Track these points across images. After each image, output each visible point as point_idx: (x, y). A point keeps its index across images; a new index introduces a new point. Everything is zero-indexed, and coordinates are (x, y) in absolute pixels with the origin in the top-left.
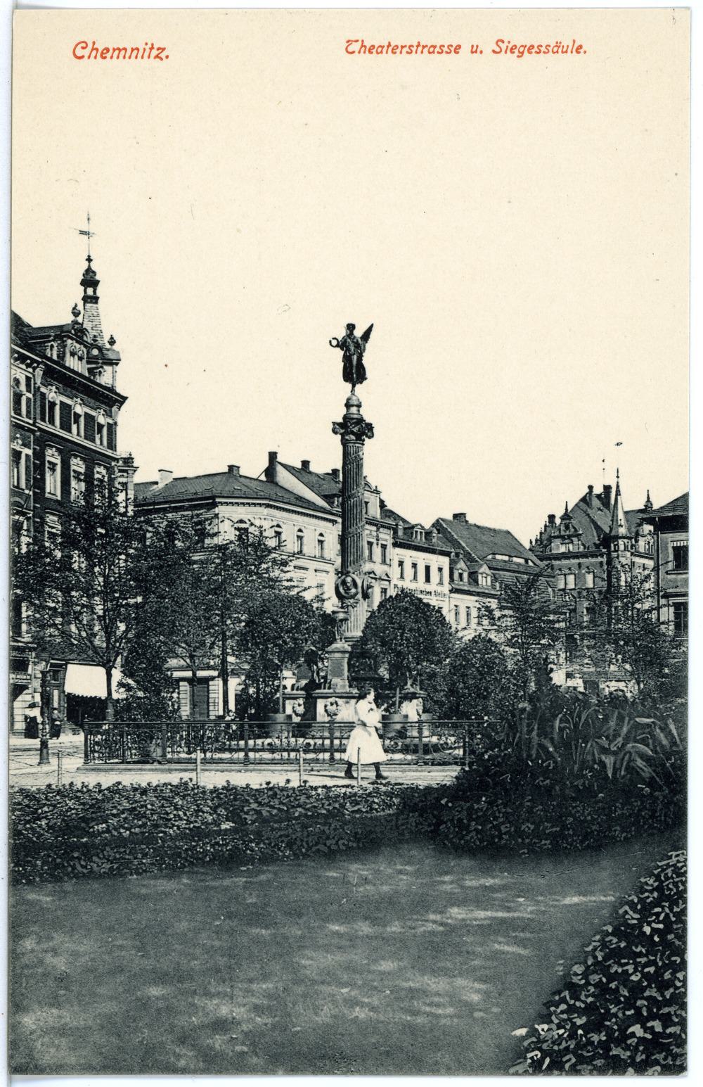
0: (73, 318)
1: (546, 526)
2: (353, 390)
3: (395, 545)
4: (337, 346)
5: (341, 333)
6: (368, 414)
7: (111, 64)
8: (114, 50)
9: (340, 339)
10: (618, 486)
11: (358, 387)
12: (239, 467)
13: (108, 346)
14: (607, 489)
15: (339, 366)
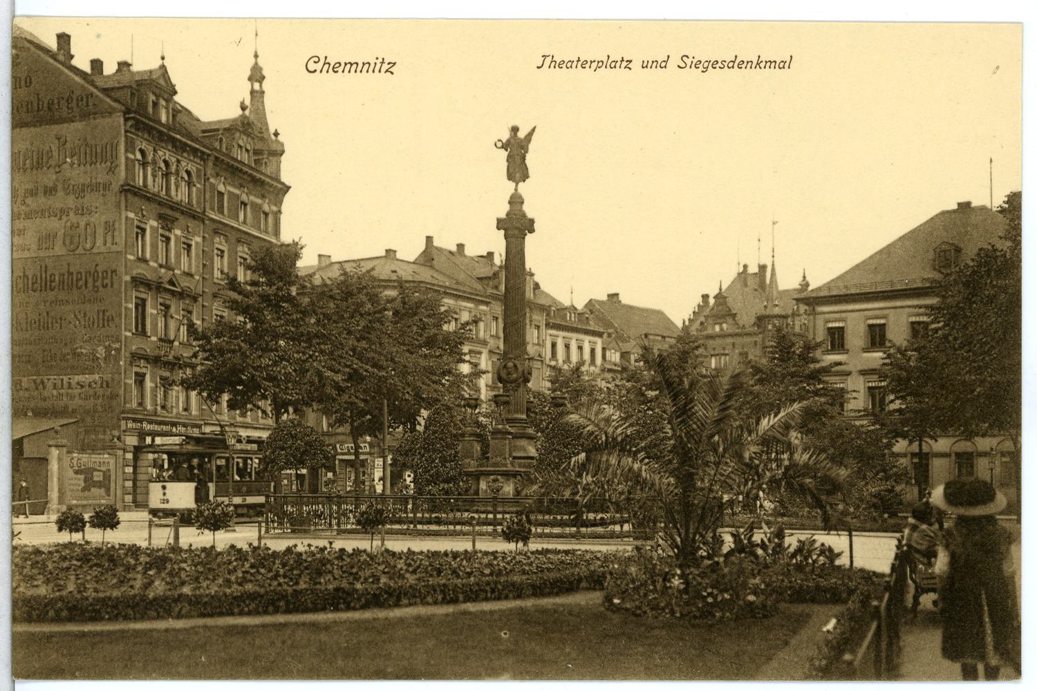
0: (240, 112)
1: (699, 306)
2: (517, 186)
3: (548, 325)
4: (502, 147)
5: (505, 136)
6: (529, 210)
7: (341, 78)
8: (346, 64)
9: (504, 141)
10: (773, 265)
11: (521, 185)
12: (395, 251)
13: (273, 137)
14: (763, 268)
15: (504, 165)
